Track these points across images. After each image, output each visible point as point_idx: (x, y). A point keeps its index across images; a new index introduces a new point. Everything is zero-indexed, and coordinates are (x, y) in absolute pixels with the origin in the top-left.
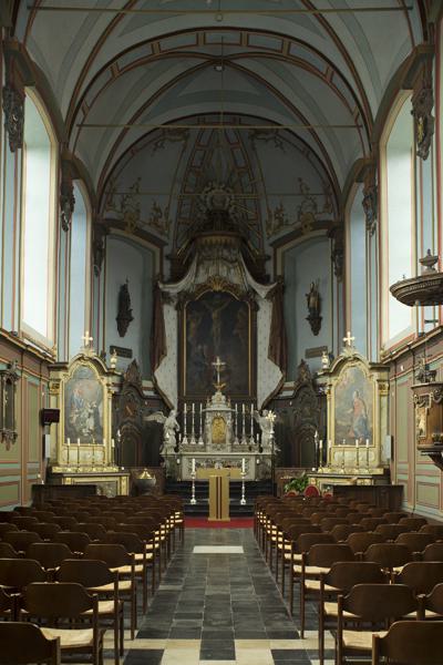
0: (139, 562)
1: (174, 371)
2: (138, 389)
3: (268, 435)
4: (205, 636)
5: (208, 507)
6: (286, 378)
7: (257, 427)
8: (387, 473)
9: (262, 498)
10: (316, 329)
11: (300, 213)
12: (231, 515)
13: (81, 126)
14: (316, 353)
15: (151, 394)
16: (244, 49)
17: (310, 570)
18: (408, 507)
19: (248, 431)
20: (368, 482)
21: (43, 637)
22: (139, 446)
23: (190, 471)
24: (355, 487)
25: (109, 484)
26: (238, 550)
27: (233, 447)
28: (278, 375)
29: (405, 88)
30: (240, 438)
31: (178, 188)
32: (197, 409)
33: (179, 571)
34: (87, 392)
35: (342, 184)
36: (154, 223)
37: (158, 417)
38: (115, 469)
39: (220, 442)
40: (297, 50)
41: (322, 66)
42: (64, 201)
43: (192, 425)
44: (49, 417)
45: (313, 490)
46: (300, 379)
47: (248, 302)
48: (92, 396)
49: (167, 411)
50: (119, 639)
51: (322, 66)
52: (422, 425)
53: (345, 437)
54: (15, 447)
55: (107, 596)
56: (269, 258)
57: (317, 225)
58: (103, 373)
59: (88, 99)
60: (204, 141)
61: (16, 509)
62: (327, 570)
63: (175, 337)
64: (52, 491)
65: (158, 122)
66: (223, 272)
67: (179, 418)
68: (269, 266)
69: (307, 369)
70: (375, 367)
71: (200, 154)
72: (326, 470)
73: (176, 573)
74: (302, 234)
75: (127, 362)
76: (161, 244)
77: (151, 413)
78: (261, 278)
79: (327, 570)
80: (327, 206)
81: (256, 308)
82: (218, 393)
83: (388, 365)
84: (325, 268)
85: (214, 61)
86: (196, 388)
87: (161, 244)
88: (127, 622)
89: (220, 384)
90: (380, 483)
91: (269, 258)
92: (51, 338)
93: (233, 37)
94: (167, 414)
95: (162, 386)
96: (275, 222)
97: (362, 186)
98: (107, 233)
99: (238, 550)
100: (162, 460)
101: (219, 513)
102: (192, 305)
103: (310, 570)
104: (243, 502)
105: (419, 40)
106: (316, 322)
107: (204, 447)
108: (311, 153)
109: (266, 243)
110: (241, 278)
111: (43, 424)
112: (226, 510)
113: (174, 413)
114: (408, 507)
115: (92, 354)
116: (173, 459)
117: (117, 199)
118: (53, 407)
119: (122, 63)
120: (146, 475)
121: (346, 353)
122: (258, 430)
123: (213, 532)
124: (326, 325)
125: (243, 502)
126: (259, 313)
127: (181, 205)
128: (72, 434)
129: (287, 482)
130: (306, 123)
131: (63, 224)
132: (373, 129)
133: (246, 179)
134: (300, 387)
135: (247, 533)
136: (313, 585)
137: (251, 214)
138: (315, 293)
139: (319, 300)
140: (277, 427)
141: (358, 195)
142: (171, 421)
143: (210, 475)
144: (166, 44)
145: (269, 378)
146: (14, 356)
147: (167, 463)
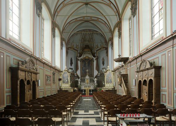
0: (74, 102)
1: (80, 72)
2: (74, 75)
3: (96, 82)
4: (85, 110)
5: (86, 93)
6: (99, 73)
7: (94, 81)
8: (114, 88)
9: (94, 92)
10: (103, 65)
11: (101, 46)
12: (89, 95)
13: (57, 16)
14: (103, 69)
15: (76, 75)
16: (91, 19)
17: (103, 106)
18: (117, 93)
19: (92, 81)
20: (111, 89)
21: (52, 120)
22: (74, 84)
23: (83, 88)
24: (109, 90)
25: (70, 90)
26: (90, 100)
27: (90, 84)
28: (97, 72)
29: (117, 27)
30: (91, 83)
31: (80, 42)
32: (84, 78)
33: (81, 103)
34: (66, 76)
35: (107, 41)
36: (76, 47)
37: (77, 79)
38: (71, 88)
39: (88, 83)
40: (99, 20)
41: (104, 22)
42: (62, 45)
43: (83, 81)
44: (60, 80)
45: (103, 91)
46: (101, 73)
47: (92, 60)
48: (67, 76)
49: (79, 78)
50: (73, 110)
51: (104, 22)
52: (119, 81)
53: (108, 82)
54: (55, 84)
55: (69, 107)
56: (95, 53)
57: (104, 48)
58: (68, 72)
59: (65, 28)
60: (84, 34)
61: (51, 95)
62: (105, 106)
63: (80, 66)
64: (61, 91)
65: (75, 32)
66: (88, 55)
67: (81, 79)
68: (96, 54)
69: (102, 71)
70: (112, 71)
71: (84, 36)
72: (105, 88)
73: (81, 103)
74: (106, 90)
75: (72, 70)
76: (77, 51)
77: (76, 79)
78: (94, 56)
79: (105, 106)
80: (105, 44)
81: (94, 61)
82: (87, 76)
83: (114, 71)
84: (105, 55)
85: (86, 21)
86: (84, 74)
87: (77, 51)
88: (74, 109)
89: (87, 74)
90: (113, 89)
91: (95, 53)
92: (60, 67)
93: (89, 18)
94: (79, 78)
95: (78, 74)
96: (97, 47)
97: (111, 42)
98: (68, 49)
99: (90, 100)
100: (78, 86)
101: (87, 95)
102: (83, 61)
103: (103, 106)
104: (91, 93)
105: (119, 20)
106: (103, 63)
107: (85, 84)
108: (102, 36)
109: (95, 50)
110: (91, 56)
111: (59, 81)
112: (88, 94)
113: (80, 79)
114: (117, 93)
115: (67, 70)
116: (80, 86)
117: (70, 44)
118: (60, 78)
119: (71, 22)
120: (76, 89)
121: (108, 69)
122: (94, 81)
123: (86, 97)
124: (105, 64)
125: (91, 93)
126: (94, 62)
127: (81, 44)
128: (64, 82)
129: (98, 89)
130: (102, 32)
131: (62, 49)
132: (112, 33)
133: (92, 40)
134: (101, 74)
135: (92, 97)
136: (103, 108)
137: (93, 46)
138: (103, 59)
139: (104, 60)
140: (97, 81)
141: (116, 33)
142: (80, 80)
143: (86, 88)
144: (78, 19)
145: (96, 73)
146: (54, 70)
147: (79, 87)
